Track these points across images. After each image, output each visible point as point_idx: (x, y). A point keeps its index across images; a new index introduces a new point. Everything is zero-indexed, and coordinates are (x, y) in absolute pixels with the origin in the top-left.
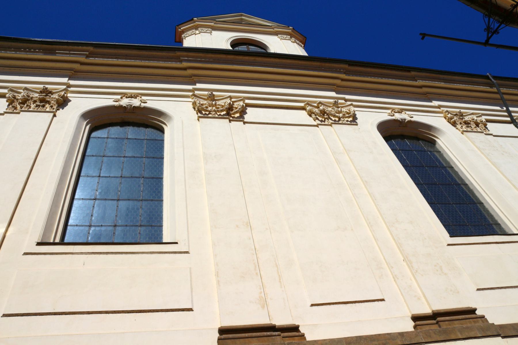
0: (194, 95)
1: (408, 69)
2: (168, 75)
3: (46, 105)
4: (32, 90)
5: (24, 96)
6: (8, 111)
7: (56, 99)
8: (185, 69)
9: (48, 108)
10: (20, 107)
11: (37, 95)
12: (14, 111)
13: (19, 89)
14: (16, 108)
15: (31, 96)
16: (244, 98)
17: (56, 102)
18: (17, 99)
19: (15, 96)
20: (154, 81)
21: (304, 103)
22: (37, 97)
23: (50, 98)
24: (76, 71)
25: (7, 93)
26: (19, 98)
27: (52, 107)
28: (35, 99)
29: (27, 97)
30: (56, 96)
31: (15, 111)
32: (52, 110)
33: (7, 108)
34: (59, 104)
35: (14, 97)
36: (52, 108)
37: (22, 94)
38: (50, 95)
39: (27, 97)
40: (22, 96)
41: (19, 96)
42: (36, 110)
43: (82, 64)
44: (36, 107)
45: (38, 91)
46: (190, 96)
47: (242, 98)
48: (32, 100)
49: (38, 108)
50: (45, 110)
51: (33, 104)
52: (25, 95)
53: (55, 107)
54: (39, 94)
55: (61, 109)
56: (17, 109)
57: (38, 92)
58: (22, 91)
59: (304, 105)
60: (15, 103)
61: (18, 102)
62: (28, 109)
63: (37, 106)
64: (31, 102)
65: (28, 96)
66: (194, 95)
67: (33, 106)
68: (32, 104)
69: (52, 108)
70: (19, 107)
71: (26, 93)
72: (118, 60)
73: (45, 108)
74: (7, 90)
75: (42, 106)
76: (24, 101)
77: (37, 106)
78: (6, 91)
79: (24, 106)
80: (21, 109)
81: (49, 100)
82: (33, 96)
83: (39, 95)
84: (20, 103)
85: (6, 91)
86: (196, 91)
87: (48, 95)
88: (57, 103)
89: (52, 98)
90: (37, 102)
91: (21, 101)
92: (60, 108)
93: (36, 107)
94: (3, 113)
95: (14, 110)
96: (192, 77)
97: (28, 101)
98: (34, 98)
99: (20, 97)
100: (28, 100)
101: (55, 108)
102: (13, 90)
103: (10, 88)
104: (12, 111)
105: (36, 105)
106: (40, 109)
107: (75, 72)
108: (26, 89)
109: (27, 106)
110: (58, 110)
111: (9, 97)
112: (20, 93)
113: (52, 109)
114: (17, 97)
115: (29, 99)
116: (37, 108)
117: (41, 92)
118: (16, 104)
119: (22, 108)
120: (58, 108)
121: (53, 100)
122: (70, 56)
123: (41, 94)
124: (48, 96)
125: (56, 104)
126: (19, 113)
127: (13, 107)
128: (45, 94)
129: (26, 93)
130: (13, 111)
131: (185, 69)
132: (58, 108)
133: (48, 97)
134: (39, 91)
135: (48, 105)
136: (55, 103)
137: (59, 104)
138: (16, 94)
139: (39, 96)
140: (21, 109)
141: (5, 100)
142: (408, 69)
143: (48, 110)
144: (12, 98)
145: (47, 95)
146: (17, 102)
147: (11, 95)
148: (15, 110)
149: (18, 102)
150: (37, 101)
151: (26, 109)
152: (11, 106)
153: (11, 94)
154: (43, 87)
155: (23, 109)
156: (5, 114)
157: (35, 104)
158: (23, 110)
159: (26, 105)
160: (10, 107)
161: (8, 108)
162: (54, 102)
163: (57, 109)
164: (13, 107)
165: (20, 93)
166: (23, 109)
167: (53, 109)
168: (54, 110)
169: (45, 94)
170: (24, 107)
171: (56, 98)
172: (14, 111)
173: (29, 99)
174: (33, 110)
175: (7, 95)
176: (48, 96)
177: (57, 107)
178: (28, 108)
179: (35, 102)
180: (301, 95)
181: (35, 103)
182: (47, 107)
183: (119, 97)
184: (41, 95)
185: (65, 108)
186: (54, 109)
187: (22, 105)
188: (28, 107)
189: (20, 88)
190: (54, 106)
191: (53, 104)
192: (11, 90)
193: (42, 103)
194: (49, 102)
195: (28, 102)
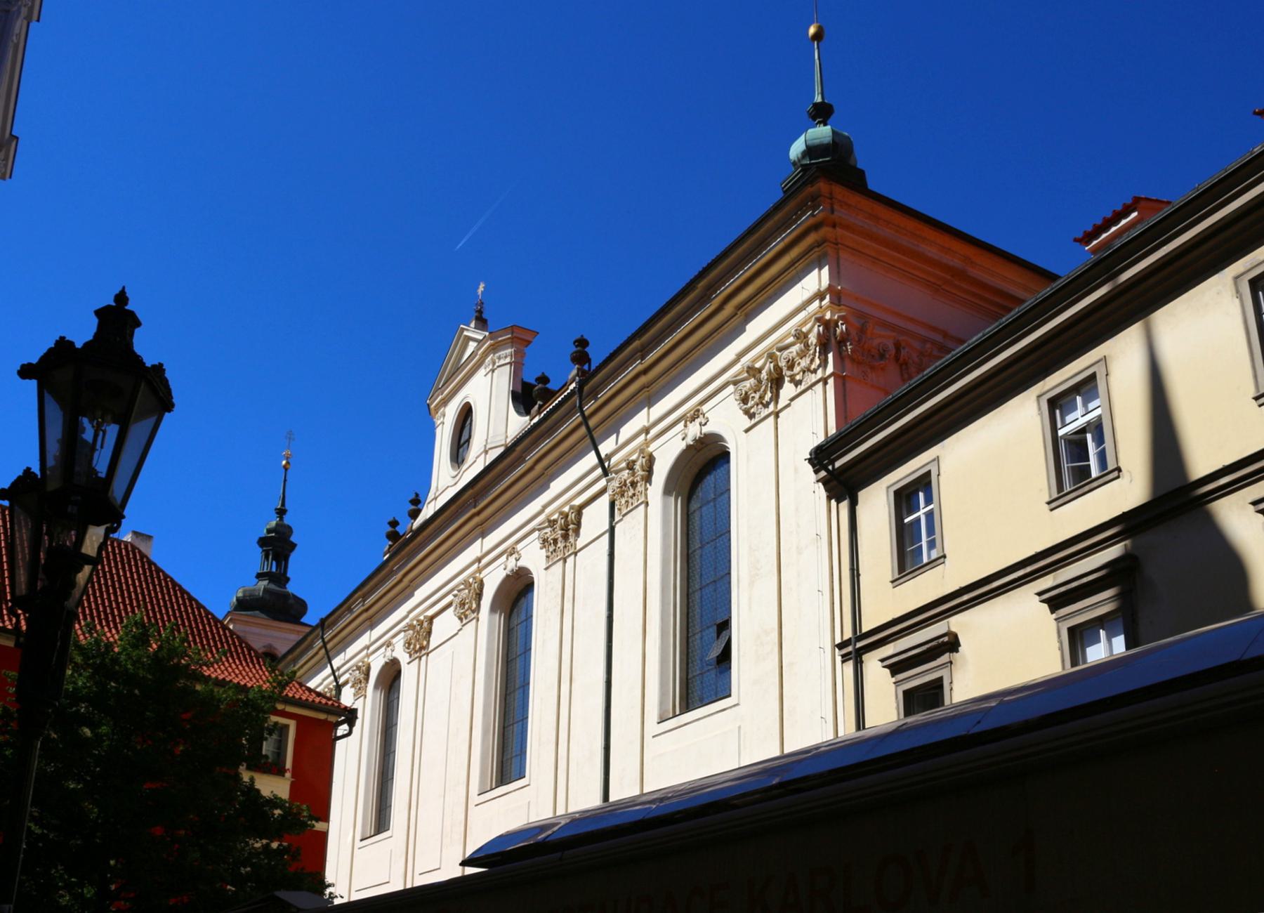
24: (370, 618)
78: (450, 598)
85: (450, 598)
107: (648, 387)
116: (799, 387)
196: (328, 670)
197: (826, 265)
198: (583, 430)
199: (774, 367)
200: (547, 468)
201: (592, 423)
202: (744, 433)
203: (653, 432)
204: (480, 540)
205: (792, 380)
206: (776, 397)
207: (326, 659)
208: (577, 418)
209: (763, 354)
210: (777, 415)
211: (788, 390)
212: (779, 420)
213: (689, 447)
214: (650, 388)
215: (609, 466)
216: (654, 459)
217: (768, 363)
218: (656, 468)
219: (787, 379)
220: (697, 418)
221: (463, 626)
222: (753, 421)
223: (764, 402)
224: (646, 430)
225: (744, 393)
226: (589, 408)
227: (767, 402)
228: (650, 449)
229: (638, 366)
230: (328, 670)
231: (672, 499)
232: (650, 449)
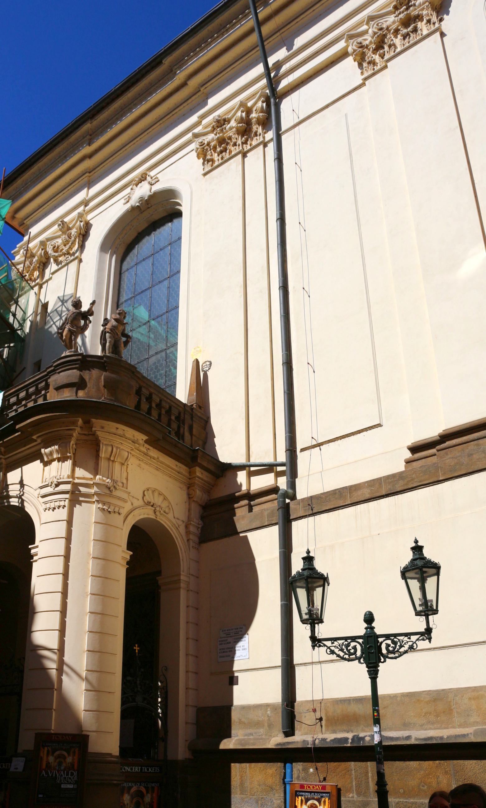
0: (196, 136)
1: (156, 62)
2: (270, 35)
3: (417, 24)
4: (378, 15)
5: (375, 33)
6: (366, 75)
7: (427, 4)
8: (184, 84)
9: (422, 26)
10: (380, 56)
11: (391, 19)
12: (376, 70)
13: (357, 28)
14: (373, 63)
15: (384, 26)
16: (262, 90)
17: (430, 9)
18: (367, 47)
19: (361, 43)
20: (66, 199)
21: (344, 38)
22: (394, 22)
23: (416, 9)
24: (90, 171)
25: (347, 47)
26: (367, 42)
27: (429, 21)
28: (394, 27)
29: (380, 32)
30: (233, 123)
31: (376, 68)
32: (433, 28)
33: (360, 71)
34: (436, 9)
35: (361, 46)
36: (430, 24)
37: (370, 31)
38: (413, 2)
39: (380, 32)
40: (372, 35)
41: (365, 40)
42: (407, 45)
43: (90, 156)
44: (404, 39)
45: (390, 9)
46: (191, 140)
47: (260, 91)
48: (392, 32)
49: (409, 38)
50: (422, 35)
51: (396, 37)
52: (376, 30)
53: (434, 19)
54: (395, 13)
55: (445, 16)
56: (377, 63)
57: (390, 10)
58: (365, 27)
59: (345, 42)
60: (368, 55)
61: (371, 50)
62: (394, 52)
63: (405, 37)
64: (391, 37)
65: (381, 29)
66: (196, 136)
67: (398, 41)
68: (394, 39)
69: (430, 24)
70: (377, 58)
71: (375, 26)
72: (156, 94)
73: (419, 32)
74: (344, 40)
75: (412, 32)
76: (379, 42)
77: (405, 37)
78: (341, 45)
79: (384, 52)
80: (383, 58)
81: (416, 13)
82: (388, 23)
83: (395, 17)
84: (375, 51)
85: (341, 45)
86: (64, 219)
87: (410, 4)
88: (259, 124)
89: (420, 5)
90: (399, 30)
91: (374, 47)
92: (443, 15)
93: (404, 39)
94: (362, 82)
95: (374, 66)
96: (200, 90)
97: (386, 38)
98: (391, 25)
99: (368, 39)
100: (385, 36)
101: (436, 21)
102: (351, 34)
103: (347, 35)
104: (373, 71)
105: (402, 35)
106: (413, 38)
107: (90, 173)
108: (371, 18)
109: (390, 46)
110: (441, 20)
111: (355, 51)
112: (366, 32)
113: (432, 25)
114: (365, 43)
115: (384, 33)
116: (407, 40)
117: (214, 129)
118: (370, 55)
119: (384, 55)
120: (439, 18)
121: (423, 9)
122: (241, 25)
123: (397, 13)
124: (411, 6)
125: (432, 13)
126: (386, 67)
127: (369, 63)
128: (405, 7)
129: (375, 26)
130: (374, 69)
131: (184, 84)
132: (439, 18)
133: (411, 8)
134: (391, 8)
135: (419, 23)
136: (430, 11)
137: (436, 9)
138: (360, 40)
139: (396, 18)
140: (383, 58)
141: (350, 59)
142: (156, 62)
143: (425, 32)
144: (360, 49)
145: (408, 5)
146: (369, 50)
147: (355, 45)
148: (375, 67)
149: (371, 50)
150: (399, 27)
151: (392, 54)
152: (365, 65)
153: (354, 44)
154: (57, 227)
155: (387, 57)
156: (367, 82)
157: (399, 36)
158: (388, 57)
159: (386, 48)
160: (365, 67)
161: (364, 70)
162: (427, 10)
163: (438, 19)
164: (369, 63)
165: (366, 32)
166: (387, 57)
167: (434, 24)
168: (437, 25)
169: (405, 7)
170: (386, 52)
171: (233, 128)
172: (376, 70)
173: (384, 33)
174: (403, 48)
175: (350, 50)
176: (411, 6)
177: (437, 17)
178: (393, 50)
179: (397, 31)
180: (156, 151)
181: (397, 34)
182: (421, 28)
183: (128, 190)
184: (400, 14)
185: (450, 9)
186: (435, 22)
187: (382, 51)
188: (393, 48)
189: (360, 24)
190: (431, 17)
191: (428, 15)
192: (351, 37)
193: (409, 26)
194: (419, 18)
195: (386, 40)
196: (259, 69)
197: (85, 188)
198: (254, 38)
199: (44, 253)
200: (203, 84)
201: (266, 29)
202: (202, 177)
203: (92, 204)
204: (86, 189)
205: (56, 261)
206: (42, 274)
207: (258, 52)
208: (249, 23)
209: (210, 125)
210: (244, 155)
211: (53, 267)
212: (81, 264)
213: (133, 209)
214: (91, 174)
215: (275, 76)
216: (91, 225)
217: (41, 249)
218: (92, 232)
219: (52, 260)
220: (144, 180)
221: (366, 79)
222: (60, 266)
223: (71, 252)
224: (85, 203)
225: (56, 245)
226: (263, 13)
227: (35, 278)
228: (89, 217)
229: (86, 150)
230: (259, 69)
231: (108, 256)
232: (89, 217)
